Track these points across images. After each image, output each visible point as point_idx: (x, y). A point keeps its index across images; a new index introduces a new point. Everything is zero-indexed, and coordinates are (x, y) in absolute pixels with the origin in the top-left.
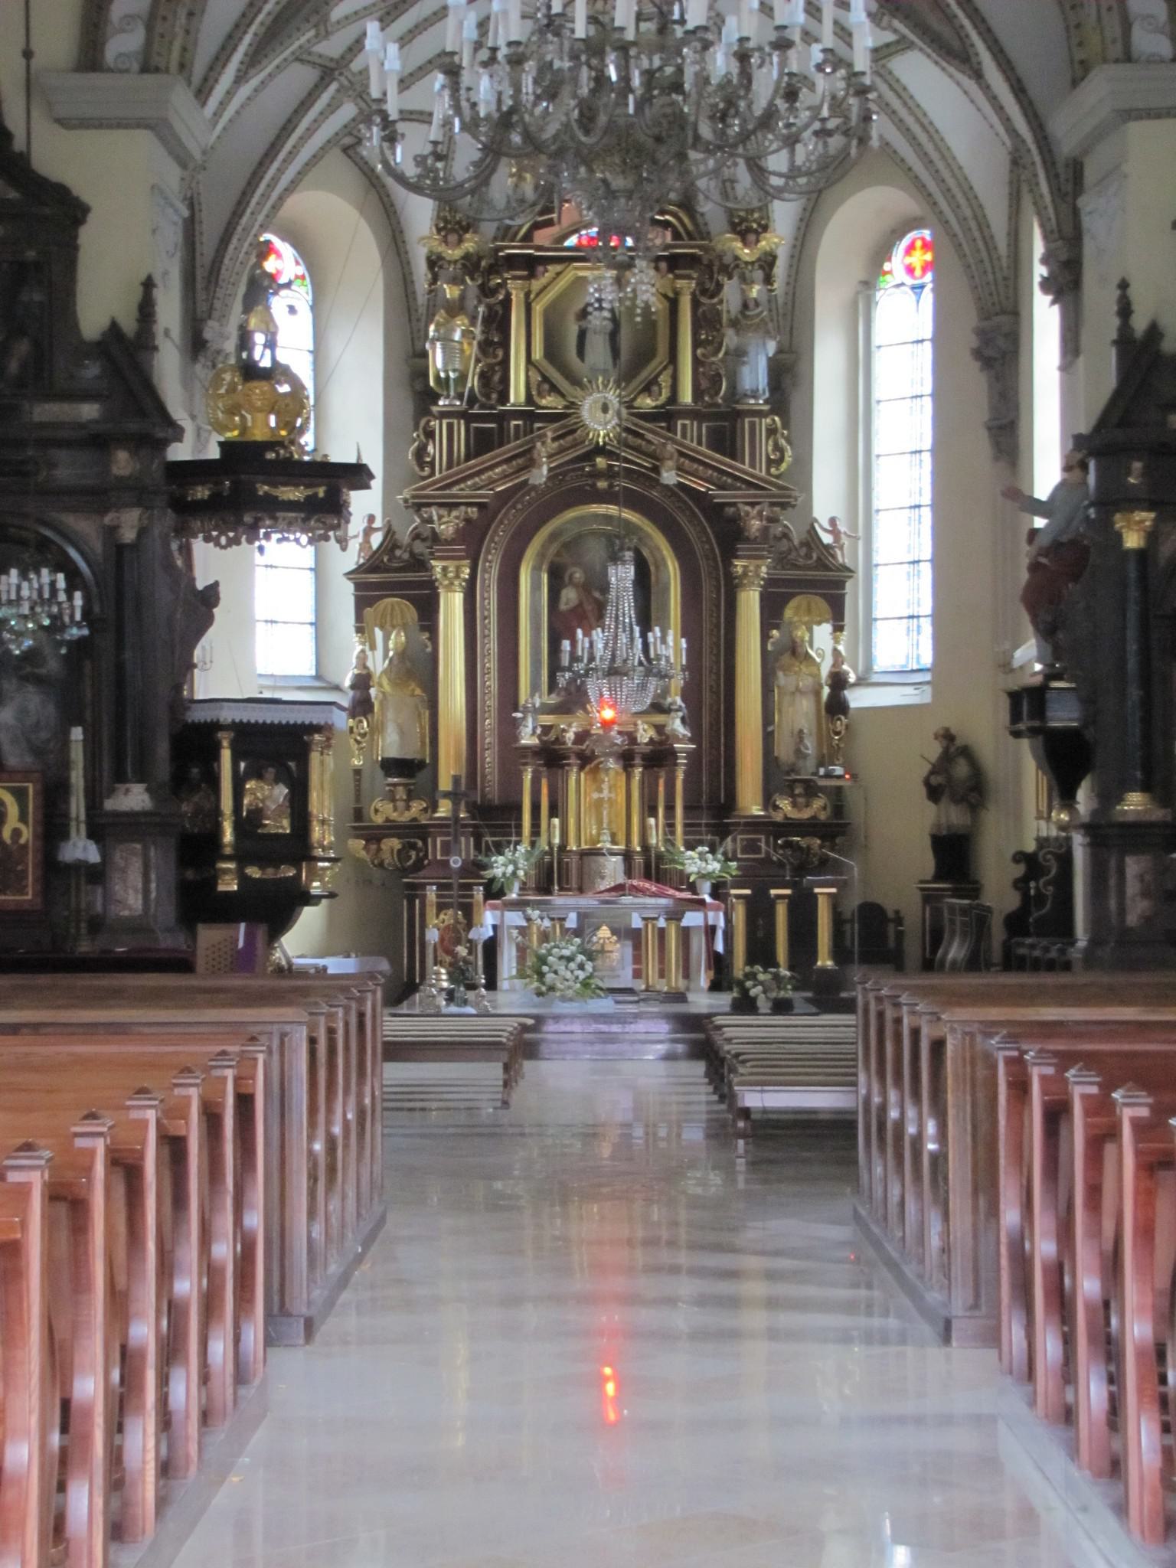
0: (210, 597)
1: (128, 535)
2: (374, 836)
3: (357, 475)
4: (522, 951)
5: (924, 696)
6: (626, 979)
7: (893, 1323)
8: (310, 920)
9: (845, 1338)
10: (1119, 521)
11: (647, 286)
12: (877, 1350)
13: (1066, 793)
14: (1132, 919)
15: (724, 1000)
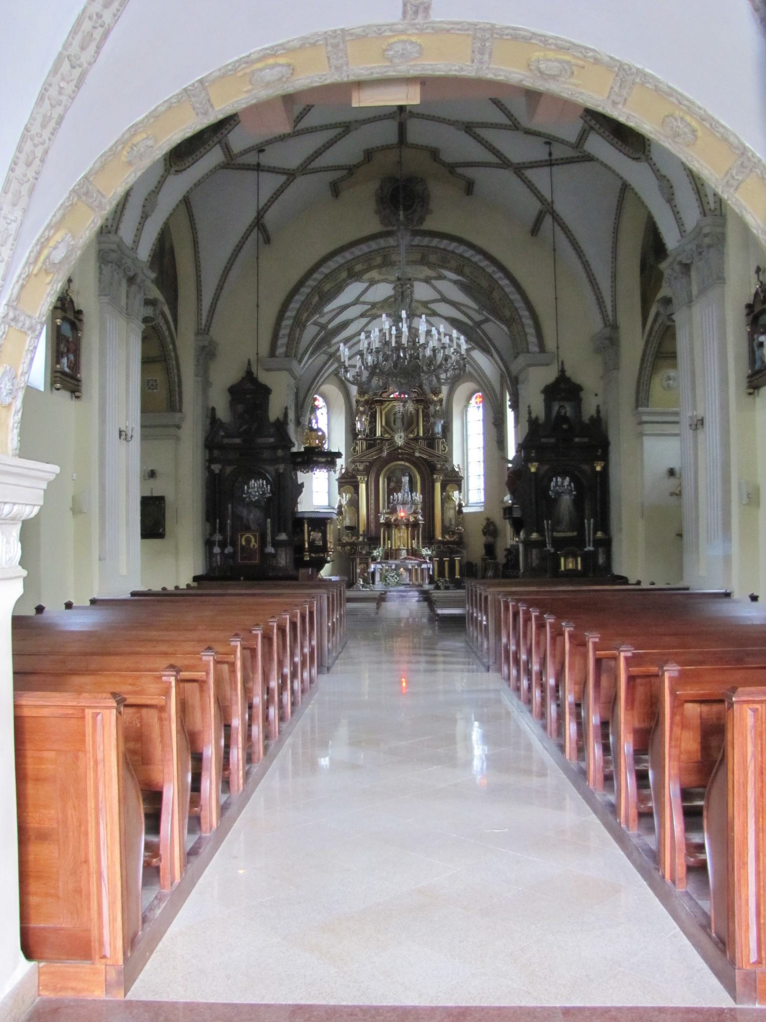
0: (302, 485)
1: (281, 471)
2: (344, 545)
3: (338, 455)
4: (381, 575)
5: (482, 509)
6: (407, 581)
7: (475, 667)
8: (327, 567)
9: (462, 671)
10: (529, 465)
11: (411, 407)
12: (470, 674)
13: (517, 533)
14: (534, 564)
15: (432, 586)
